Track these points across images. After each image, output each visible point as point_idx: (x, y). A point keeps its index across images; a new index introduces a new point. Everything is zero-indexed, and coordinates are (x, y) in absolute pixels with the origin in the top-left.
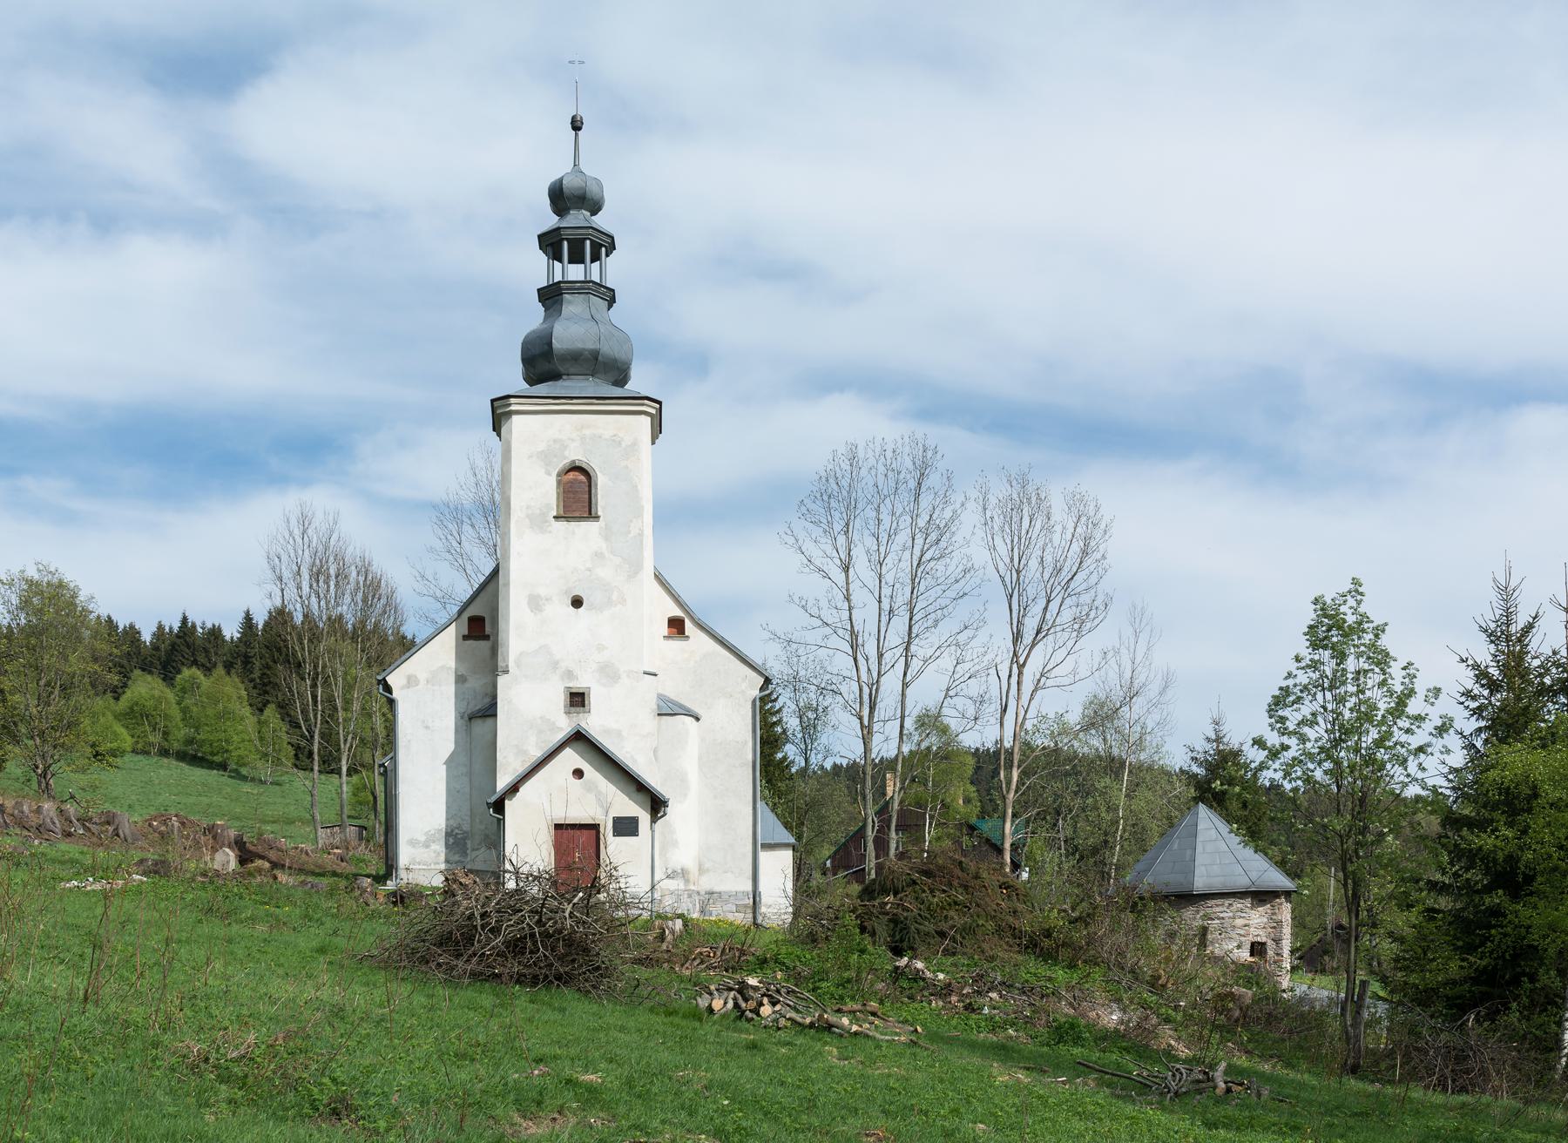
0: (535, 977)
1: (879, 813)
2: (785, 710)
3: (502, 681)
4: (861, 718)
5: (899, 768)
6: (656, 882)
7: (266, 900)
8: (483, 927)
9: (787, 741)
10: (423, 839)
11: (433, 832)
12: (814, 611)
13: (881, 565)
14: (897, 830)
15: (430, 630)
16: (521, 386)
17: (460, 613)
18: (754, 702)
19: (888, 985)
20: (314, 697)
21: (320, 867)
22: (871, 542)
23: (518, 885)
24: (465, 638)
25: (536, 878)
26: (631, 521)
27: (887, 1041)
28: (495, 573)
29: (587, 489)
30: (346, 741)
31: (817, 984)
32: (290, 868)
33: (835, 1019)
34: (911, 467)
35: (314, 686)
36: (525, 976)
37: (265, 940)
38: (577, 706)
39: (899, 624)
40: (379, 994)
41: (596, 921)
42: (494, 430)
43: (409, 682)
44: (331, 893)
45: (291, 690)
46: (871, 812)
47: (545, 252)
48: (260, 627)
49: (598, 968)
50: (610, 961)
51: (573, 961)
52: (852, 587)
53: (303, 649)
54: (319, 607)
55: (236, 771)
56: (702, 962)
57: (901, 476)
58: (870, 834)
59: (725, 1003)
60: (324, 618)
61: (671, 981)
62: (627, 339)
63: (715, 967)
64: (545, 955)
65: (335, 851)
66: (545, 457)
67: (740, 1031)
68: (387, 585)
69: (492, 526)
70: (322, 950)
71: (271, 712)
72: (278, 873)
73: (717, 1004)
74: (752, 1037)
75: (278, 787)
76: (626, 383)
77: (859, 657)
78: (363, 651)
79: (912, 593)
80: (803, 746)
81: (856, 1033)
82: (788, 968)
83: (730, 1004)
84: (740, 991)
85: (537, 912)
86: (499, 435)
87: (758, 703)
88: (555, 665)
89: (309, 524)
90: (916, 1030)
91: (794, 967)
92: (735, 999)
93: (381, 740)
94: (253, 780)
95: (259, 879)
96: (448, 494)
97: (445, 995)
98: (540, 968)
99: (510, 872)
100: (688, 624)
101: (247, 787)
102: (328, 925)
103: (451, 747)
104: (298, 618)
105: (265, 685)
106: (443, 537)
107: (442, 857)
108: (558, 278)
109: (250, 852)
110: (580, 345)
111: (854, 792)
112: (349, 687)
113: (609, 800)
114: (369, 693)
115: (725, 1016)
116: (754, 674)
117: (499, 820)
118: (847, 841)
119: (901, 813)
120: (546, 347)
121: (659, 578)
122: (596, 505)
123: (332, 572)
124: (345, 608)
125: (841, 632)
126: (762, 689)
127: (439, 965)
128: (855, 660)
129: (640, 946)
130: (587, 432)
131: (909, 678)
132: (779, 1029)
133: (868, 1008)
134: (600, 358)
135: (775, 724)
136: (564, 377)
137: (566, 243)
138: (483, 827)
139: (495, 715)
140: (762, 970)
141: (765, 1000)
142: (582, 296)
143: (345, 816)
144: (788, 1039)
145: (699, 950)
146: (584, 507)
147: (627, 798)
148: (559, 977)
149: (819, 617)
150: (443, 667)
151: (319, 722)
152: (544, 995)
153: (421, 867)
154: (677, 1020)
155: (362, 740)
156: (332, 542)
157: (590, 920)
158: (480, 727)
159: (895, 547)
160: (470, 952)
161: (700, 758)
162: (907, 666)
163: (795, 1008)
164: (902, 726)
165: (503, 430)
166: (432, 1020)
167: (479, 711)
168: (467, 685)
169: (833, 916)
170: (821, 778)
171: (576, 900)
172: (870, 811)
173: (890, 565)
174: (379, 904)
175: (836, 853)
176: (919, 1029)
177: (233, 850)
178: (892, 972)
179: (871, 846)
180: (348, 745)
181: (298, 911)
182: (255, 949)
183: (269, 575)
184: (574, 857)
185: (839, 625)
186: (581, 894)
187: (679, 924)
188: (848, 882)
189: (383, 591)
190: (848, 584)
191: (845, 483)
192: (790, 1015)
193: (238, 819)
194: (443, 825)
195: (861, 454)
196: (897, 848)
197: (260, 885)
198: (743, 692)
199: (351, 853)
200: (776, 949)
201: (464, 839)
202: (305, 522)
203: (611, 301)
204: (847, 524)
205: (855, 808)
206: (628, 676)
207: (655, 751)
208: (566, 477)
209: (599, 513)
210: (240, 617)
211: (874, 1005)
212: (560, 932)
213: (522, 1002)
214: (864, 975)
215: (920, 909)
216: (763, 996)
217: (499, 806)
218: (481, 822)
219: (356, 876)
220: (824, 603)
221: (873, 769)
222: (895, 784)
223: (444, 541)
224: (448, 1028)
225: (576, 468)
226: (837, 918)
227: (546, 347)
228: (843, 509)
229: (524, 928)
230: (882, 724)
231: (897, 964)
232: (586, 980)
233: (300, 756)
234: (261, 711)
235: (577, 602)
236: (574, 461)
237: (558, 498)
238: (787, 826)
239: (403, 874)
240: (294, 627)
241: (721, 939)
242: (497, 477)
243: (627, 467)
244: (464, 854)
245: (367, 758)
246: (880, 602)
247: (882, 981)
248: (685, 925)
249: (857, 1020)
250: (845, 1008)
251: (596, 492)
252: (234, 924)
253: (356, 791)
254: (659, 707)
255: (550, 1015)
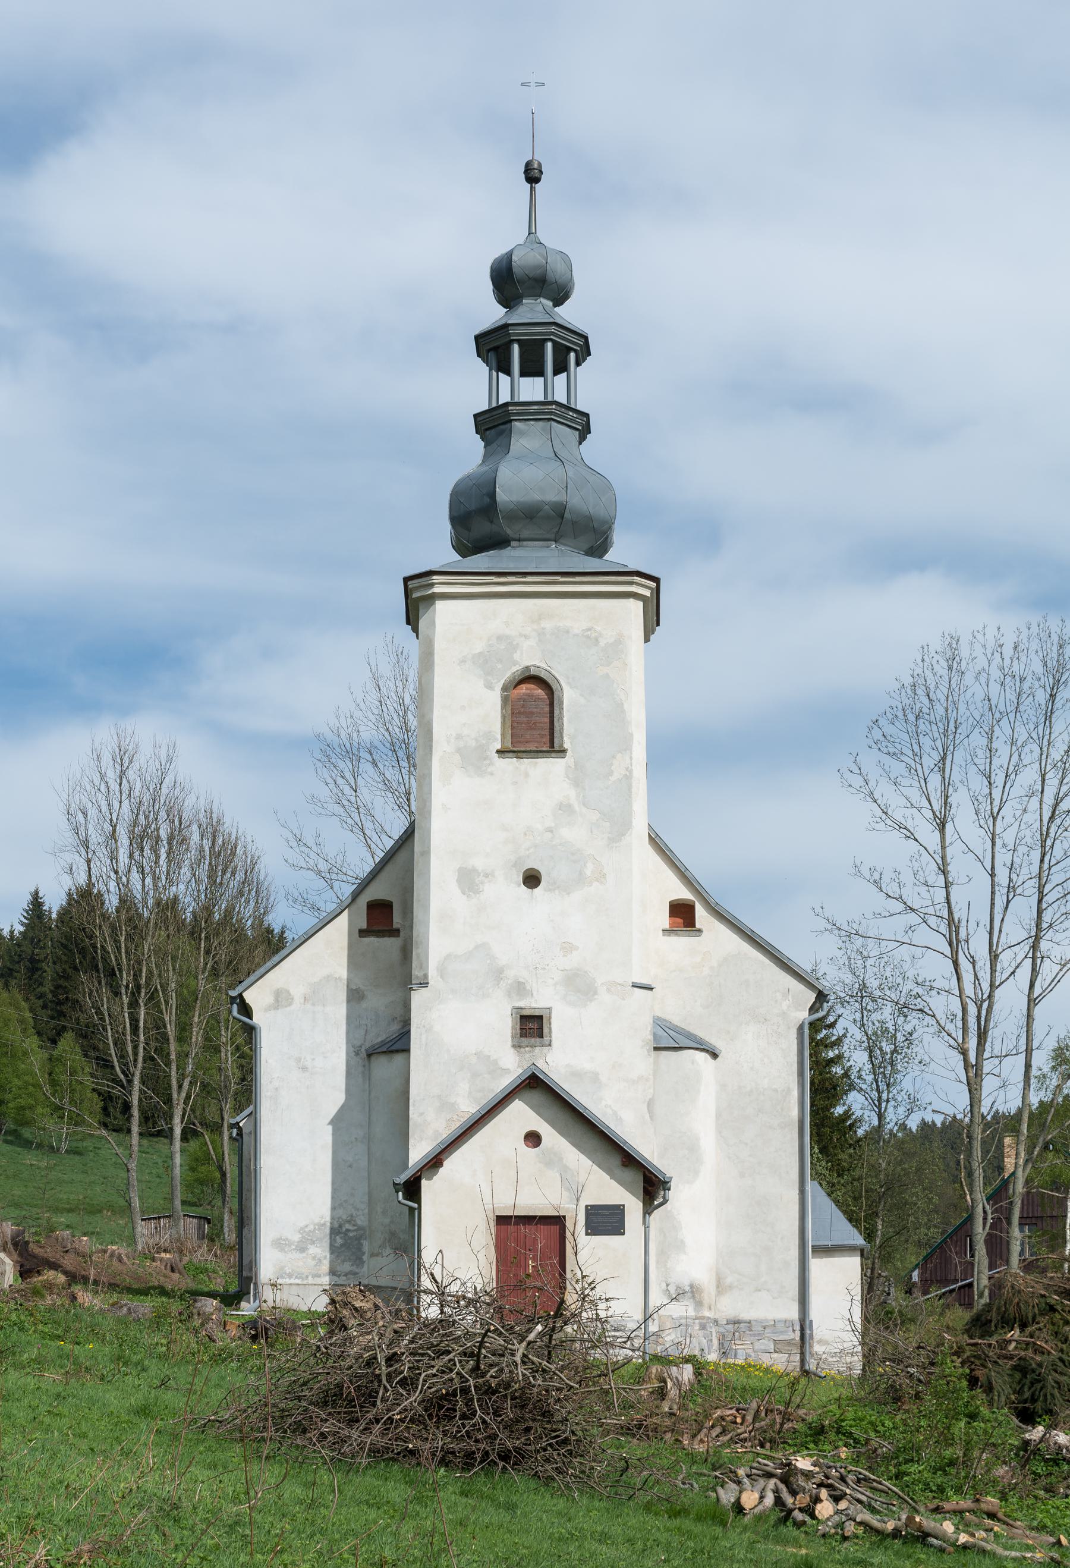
0: (470, 1455)
1: (993, 1198)
2: (846, 1041)
3: (418, 998)
4: (964, 1053)
5: (1024, 1127)
6: (651, 1309)
7: (60, 1332)
8: (389, 1376)
9: (852, 1087)
10: (296, 1237)
11: (311, 1227)
12: (893, 889)
13: (995, 819)
14: (1021, 1225)
15: (311, 921)
16: (448, 557)
17: (356, 895)
18: (801, 1028)
19: (1013, 1469)
20: (134, 1021)
21: (138, 1279)
22: (979, 784)
23: (442, 1312)
24: (363, 933)
25: (470, 1302)
26: (614, 757)
27: (1014, 1559)
28: (409, 835)
29: (547, 709)
30: (180, 1087)
31: (903, 1468)
32: (96, 1282)
33: (932, 1524)
34: (1039, 669)
35: (134, 1004)
36: (453, 1453)
37: (58, 1395)
38: (531, 1036)
39: (1024, 908)
40: (231, 1483)
41: (562, 1369)
42: (408, 622)
43: (277, 1000)
44: (158, 1321)
45: (99, 1012)
46: (980, 1196)
47: (486, 361)
48: (54, 916)
49: (566, 1441)
50: (584, 1430)
51: (528, 1430)
52: (949, 851)
53: (119, 948)
54: (144, 886)
55: (14, 1133)
56: (724, 1432)
57: (1026, 686)
58: (980, 1231)
59: (762, 1498)
60: (150, 902)
61: (677, 1462)
62: (607, 486)
63: (745, 1440)
64: (484, 1422)
65: (163, 1255)
66: (484, 662)
67: (785, 1542)
68: (245, 853)
69: (404, 764)
70: (143, 1411)
71: (68, 1044)
72: (77, 1289)
73: (749, 1499)
74: (804, 1551)
75: (77, 1158)
76: (606, 551)
77: (962, 960)
78: (207, 952)
79: (1042, 861)
80: (874, 1095)
81: (965, 1547)
82: (857, 1441)
83: (769, 1500)
84: (785, 1480)
85: (472, 1355)
86: (416, 630)
87: (807, 1031)
88: (498, 974)
89: (131, 762)
90: (1059, 1542)
91: (867, 1441)
92: (776, 1491)
93: (234, 1087)
94: (40, 1146)
95: (49, 1300)
96: (338, 718)
97: (332, 1485)
98: (477, 1441)
99: (431, 1293)
100: (700, 911)
101: (31, 1158)
102: (153, 1371)
103: (340, 1098)
104: (112, 902)
105: (60, 1003)
106: (330, 781)
107: (325, 1267)
108: (504, 397)
109: (34, 1256)
110: (536, 497)
111: (952, 1164)
112: (186, 1007)
113: (582, 1179)
114: (215, 1017)
115: (760, 1518)
116: (801, 987)
117: (411, 1210)
118: (945, 1241)
119: (1028, 1197)
120: (487, 500)
121: (656, 842)
122: (561, 733)
123: (163, 834)
124: (182, 887)
125: (933, 921)
126: (813, 1009)
127: (323, 1436)
128: (956, 964)
129: (628, 1406)
130: (548, 625)
131: (1037, 990)
132: (845, 1538)
133: (983, 1506)
134: (567, 515)
135: (831, 1062)
136: (513, 543)
137: (516, 348)
138: (387, 1221)
139: (407, 1050)
140: (816, 1443)
141: (824, 1493)
142: (541, 423)
143: (177, 1203)
144: (859, 1554)
145: (719, 1413)
146: (542, 736)
147: (606, 1177)
148: (505, 1457)
149: (900, 898)
150: (328, 978)
151: (140, 1059)
152: (482, 1483)
153: (293, 1281)
154: (687, 1524)
155: (204, 1086)
156: (165, 790)
157: (553, 1367)
158: (384, 1067)
159: (1017, 791)
160: (370, 1416)
161: (718, 1115)
162: (1035, 972)
163: (870, 1505)
164: (1028, 1066)
165: (422, 624)
166: (313, 1523)
167: (383, 1043)
168: (364, 1004)
169: (927, 1361)
170: (903, 1142)
171: (531, 1337)
172: (979, 1199)
173: (1009, 819)
174: (230, 1338)
175: (926, 1259)
176: (1064, 1541)
177: (9, 1255)
178: (1019, 1449)
179: (981, 1249)
180: (184, 1095)
181: (107, 1350)
182: (43, 1409)
183: (70, 839)
184: (526, 1266)
185: (931, 910)
186: (539, 1328)
187: (687, 1372)
188: (947, 1306)
189: (239, 861)
190: (943, 848)
191: (940, 695)
192: (865, 1516)
193: (17, 1205)
194: (328, 1218)
195: (964, 652)
196: (1021, 1253)
197: (51, 1310)
198: (784, 1015)
199: (186, 1259)
200: (838, 1412)
201: (359, 1239)
202: (123, 760)
203: (584, 431)
204: (943, 759)
205: (955, 1190)
206: (609, 990)
207: (650, 1104)
208: (515, 691)
209: (566, 746)
210: (24, 901)
211: (991, 1501)
212: (508, 1386)
213: (449, 1494)
214: (976, 1453)
215: (1062, 1351)
216: (820, 1485)
217: (412, 1189)
218: (384, 1212)
219: (196, 1294)
220: (907, 877)
221: (984, 1131)
222: (1017, 1155)
223: (332, 786)
224: (338, 1536)
225: (531, 678)
226: (932, 1364)
227: (487, 500)
228: (936, 735)
229: (451, 1380)
230: (996, 1061)
231: (1027, 1436)
232: (548, 1461)
233: (111, 1110)
234: (54, 1042)
235: (532, 879)
236: (527, 668)
237: (503, 723)
238: (852, 1218)
239: (267, 1294)
240: (105, 917)
241: (753, 1396)
242: (412, 689)
243: (607, 676)
244: (359, 1261)
245: (211, 1114)
246: (993, 875)
247: (1005, 1463)
248: (698, 1373)
249: (967, 1525)
250: (947, 1506)
251: (561, 713)
252: (11, 1371)
253: (195, 1163)
254: (656, 1037)
255: (496, 1517)
